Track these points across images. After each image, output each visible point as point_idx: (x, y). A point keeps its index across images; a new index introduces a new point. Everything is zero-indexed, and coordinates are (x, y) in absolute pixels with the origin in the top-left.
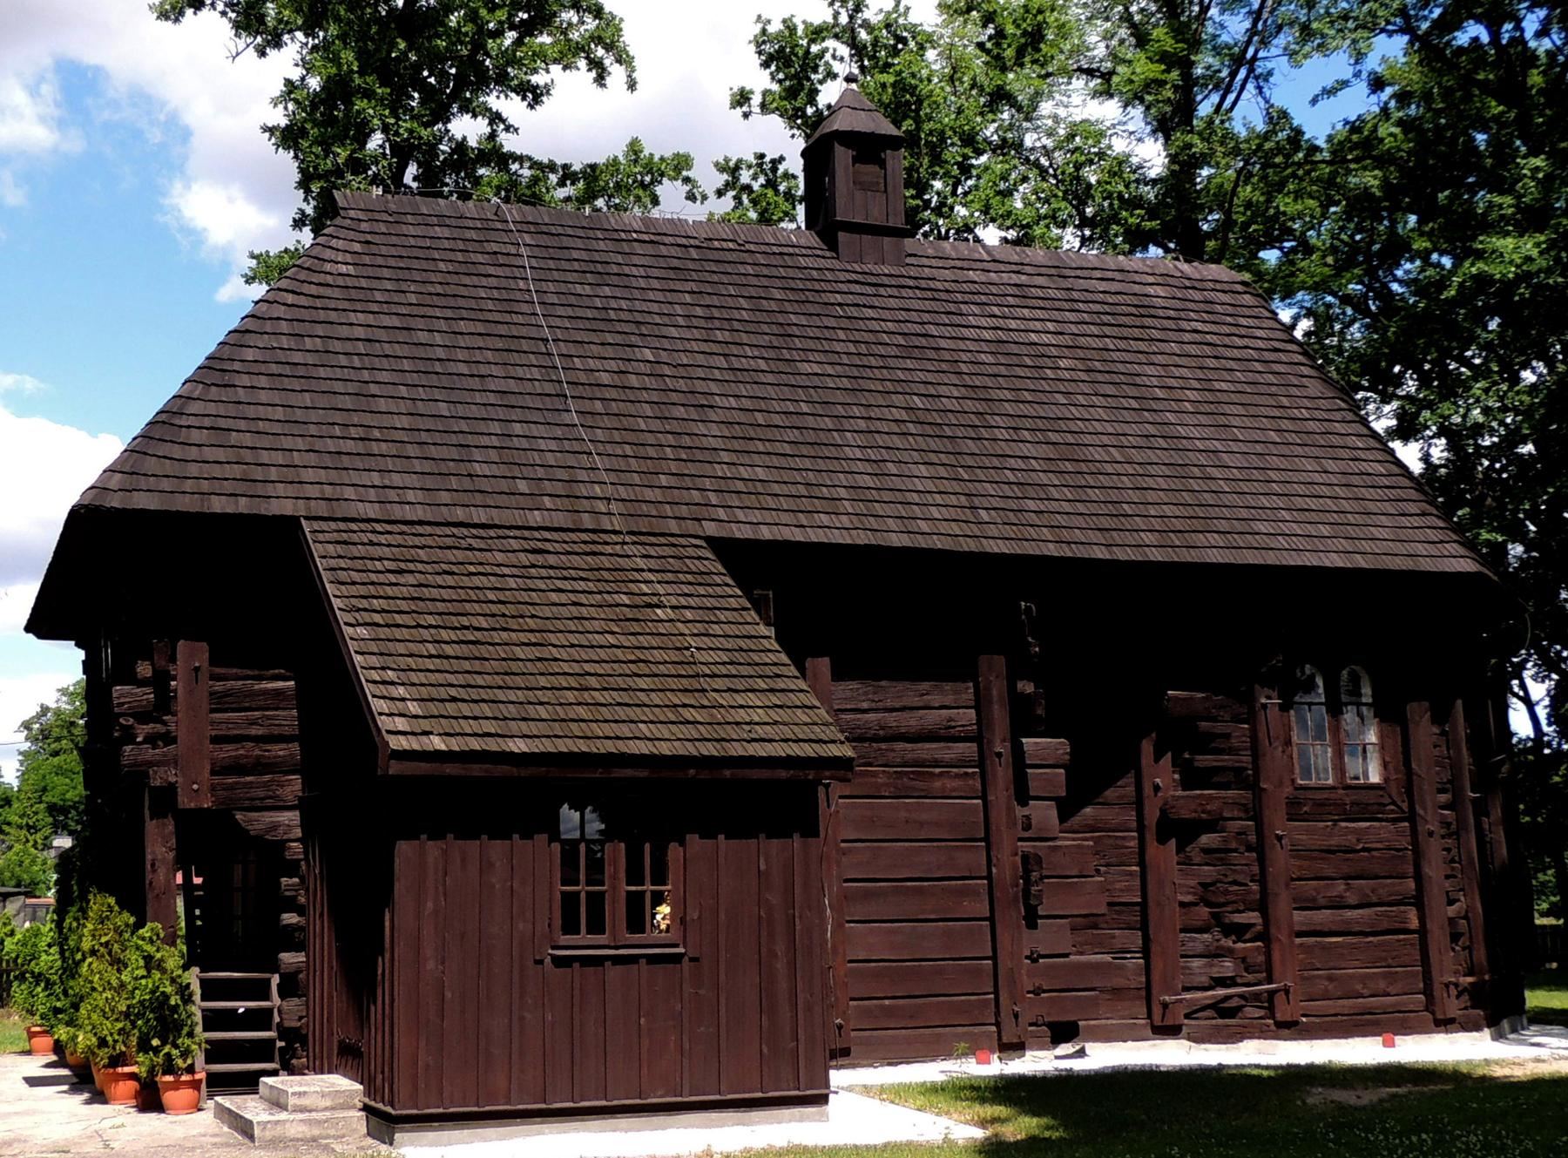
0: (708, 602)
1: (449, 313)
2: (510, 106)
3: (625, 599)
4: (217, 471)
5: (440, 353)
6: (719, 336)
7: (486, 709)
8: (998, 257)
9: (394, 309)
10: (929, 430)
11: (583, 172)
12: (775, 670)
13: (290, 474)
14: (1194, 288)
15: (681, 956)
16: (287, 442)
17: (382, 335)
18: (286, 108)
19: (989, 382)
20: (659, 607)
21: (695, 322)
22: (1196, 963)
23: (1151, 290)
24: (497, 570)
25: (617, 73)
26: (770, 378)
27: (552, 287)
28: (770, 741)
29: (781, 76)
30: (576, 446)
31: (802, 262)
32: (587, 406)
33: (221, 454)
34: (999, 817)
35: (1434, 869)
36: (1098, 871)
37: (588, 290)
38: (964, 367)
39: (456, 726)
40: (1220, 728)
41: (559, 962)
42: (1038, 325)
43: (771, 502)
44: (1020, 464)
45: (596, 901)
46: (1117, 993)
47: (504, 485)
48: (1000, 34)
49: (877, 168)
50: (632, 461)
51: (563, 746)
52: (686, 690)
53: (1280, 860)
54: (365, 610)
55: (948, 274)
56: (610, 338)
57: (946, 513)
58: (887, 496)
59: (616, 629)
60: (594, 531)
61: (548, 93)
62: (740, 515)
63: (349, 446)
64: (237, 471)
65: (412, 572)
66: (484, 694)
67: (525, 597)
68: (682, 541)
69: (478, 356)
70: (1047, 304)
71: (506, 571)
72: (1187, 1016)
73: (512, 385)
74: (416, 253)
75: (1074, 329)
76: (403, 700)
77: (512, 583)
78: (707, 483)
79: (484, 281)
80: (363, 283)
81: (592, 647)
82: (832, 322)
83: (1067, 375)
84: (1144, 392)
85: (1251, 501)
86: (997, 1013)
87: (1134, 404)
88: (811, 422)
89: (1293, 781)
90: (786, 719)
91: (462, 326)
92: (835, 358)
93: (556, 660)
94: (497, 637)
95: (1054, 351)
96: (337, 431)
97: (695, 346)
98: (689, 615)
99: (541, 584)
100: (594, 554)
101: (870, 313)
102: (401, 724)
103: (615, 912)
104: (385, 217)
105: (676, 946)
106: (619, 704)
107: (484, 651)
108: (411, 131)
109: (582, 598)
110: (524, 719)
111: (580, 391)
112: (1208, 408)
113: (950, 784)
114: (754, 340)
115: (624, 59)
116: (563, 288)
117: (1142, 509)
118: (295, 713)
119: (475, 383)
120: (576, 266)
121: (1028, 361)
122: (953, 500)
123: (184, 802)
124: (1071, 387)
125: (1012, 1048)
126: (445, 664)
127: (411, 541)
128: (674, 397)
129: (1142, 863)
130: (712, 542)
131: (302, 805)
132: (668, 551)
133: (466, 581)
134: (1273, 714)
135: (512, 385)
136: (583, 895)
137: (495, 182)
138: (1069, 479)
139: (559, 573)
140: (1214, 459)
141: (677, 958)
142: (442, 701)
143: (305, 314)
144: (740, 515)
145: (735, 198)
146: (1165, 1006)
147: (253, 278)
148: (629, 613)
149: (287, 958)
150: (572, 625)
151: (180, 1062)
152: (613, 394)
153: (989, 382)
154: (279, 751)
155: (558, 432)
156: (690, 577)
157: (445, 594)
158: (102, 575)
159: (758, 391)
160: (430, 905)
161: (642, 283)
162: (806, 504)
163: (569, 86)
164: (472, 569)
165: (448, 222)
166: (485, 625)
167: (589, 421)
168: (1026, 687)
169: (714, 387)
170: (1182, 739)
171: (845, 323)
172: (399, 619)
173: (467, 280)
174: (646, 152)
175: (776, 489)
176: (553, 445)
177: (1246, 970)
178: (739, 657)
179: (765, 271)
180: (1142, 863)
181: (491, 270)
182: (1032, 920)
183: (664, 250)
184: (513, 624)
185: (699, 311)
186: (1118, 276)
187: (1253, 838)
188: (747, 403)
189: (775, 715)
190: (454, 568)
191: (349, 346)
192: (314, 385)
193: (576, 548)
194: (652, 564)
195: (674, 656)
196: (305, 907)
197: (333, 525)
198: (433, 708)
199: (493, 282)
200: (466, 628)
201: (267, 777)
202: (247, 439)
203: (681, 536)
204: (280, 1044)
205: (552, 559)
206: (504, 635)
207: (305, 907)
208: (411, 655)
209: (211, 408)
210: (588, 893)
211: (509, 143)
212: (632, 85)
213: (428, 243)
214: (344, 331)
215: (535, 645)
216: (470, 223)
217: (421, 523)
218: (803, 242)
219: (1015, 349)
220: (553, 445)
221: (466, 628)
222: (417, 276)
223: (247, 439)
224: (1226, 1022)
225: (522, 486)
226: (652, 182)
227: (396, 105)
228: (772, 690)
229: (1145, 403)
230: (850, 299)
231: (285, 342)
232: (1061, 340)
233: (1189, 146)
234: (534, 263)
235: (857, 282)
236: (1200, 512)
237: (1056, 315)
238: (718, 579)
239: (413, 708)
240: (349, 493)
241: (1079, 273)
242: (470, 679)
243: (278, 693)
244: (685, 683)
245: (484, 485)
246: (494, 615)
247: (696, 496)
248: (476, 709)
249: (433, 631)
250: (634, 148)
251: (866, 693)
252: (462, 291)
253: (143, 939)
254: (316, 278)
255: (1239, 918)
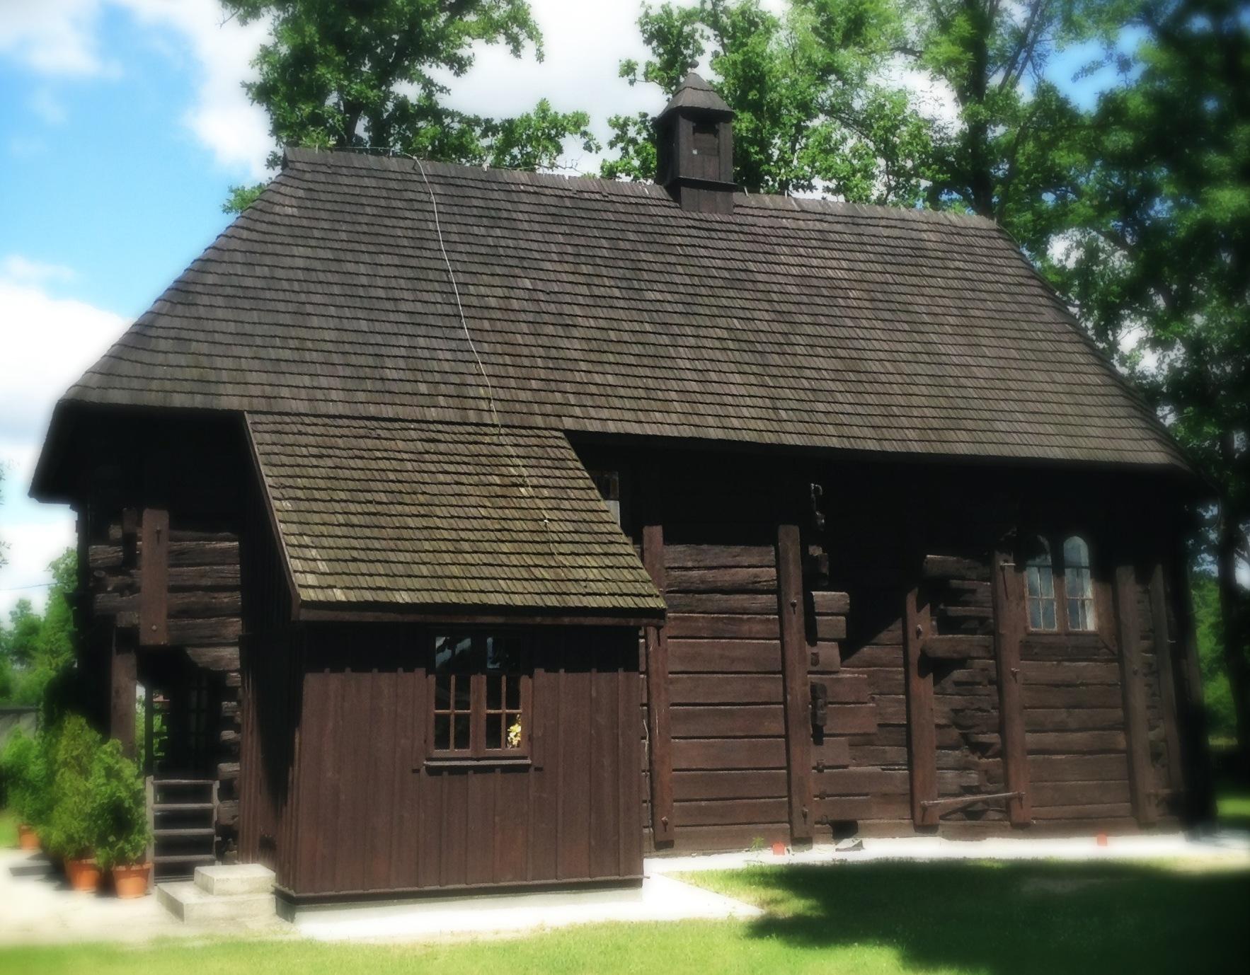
0: (562, 483)
1: (372, 248)
2: (439, 73)
3: (497, 480)
4: (178, 373)
5: (364, 280)
6: (584, 269)
7: (380, 568)
8: (806, 208)
9: (329, 244)
10: (744, 346)
11: (503, 126)
12: (610, 538)
13: (238, 376)
14: (959, 234)
15: (528, 766)
16: (237, 351)
17: (317, 265)
18: (261, 69)
19: (793, 308)
20: (522, 486)
21: (566, 258)
22: (950, 774)
23: (924, 236)
24: (399, 456)
25: (529, 47)
26: (622, 303)
27: (454, 228)
28: (600, 595)
29: (661, 51)
30: (467, 356)
31: (653, 210)
32: (476, 324)
33: (183, 360)
34: (793, 654)
35: (1139, 698)
36: (873, 699)
37: (483, 231)
38: (775, 297)
39: (354, 581)
40: (967, 585)
41: (433, 771)
42: (834, 263)
43: (617, 402)
44: (814, 374)
45: (463, 721)
46: (887, 798)
47: (408, 387)
48: (830, 22)
49: (712, 137)
50: (510, 369)
51: (438, 598)
52: (539, 554)
53: (1016, 693)
54: (291, 487)
55: (766, 222)
56: (498, 270)
57: (754, 413)
58: (709, 399)
59: (488, 504)
60: (477, 425)
61: (470, 64)
62: (593, 412)
63: (287, 354)
64: (195, 373)
65: (330, 456)
66: (379, 556)
67: (418, 477)
68: (547, 433)
69: (393, 283)
70: (843, 246)
71: (405, 456)
72: (942, 817)
73: (419, 307)
74: (349, 199)
75: (862, 266)
76: (315, 560)
77: (409, 466)
78: (568, 387)
79: (402, 223)
80: (305, 223)
81: (468, 518)
82: (673, 259)
83: (855, 303)
84: (915, 317)
85: (993, 405)
86: (790, 814)
87: (906, 327)
88: (652, 338)
89: (1026, 628)
90: (615, 577)
91: (383, 259)
92: (673, 288)
93: (438, 528)
94: (395, 509)
95: (846, 284)
96: (278, 342)
97: (565, 277)
98: (546, 492)
99: (432, 468)
100: (476, 443)
101: (703, 252)
102: (311, 579)
103: (478, 730)
104: (324, 169)
105: (525, 758)
106: (485, 564)
107: (383, 521)
108: (360, 92)
109: (464, 479)
110: (409, 576)
111: (473, 312)
112: (964, 331)
113: (757, 628)
114: (612, 272)
115: (534, 35)
116: (464, 229)
117: (907, 411)
118: (238, 567)
119: (389, 305)
120: (475, 211)
121: (825, 292)
122: (760, 402)
123: (147, 639)
124: (856, 313)
125: (802, 840)
126: (351, 532)
127: (333, 431)
128: (546, 318)
129: (907, 692)
130: (569, 434)
131: (243, 643)
132: (534, 441)
133: (373, 464)
134: (1010, 575)
135: (419, 307)
136: (452, 717)
137: (430, 134)
138: (852, 387)
139: (446, 458)
140: (965, 372)
141: (525, 768)
142: (346, 561)
143: (257, 247)
144: (593, 412)
145: (622, 149)
146: (925, 809)
147: (230, 209)
148: (498, 490)
149: (227, 768)
150: (453, 501)
151: (131, 854)
152: (498, 315)
153: (793, 308)
154: (225, 598)
155: (453, 345)
156: (549, 463)
157: (356, 474)
158: (92, 451)
159: (612, 313)
160: (331, 725)
161: (526, 226)
162: (644, 404)
163: (488, 57)
164: (378, 454)
165: (375, 174)
166: (385, 500)
167: (478, 336)
168: (816, 551)
169: (577, 311)
170: (939, 593)
171: (683, 260)
172: (317, 494)
173: (388, 222)
174: (552, 111)
175: (622, 392)
176: (449, 355)
177: (988, 781)
178: (583, 527)
179: (623, 218)
180: (907, 692)
181: (408, 214)
182: (818, 736)
183: (545, 200)
184: (407, 499)
185: (570, 249)
186: (899, 224)
187: (993, 673)
188: (602, 323)
189: (607, 574)
190: (365, 454)
191: (291, 274)
192: (261, 304)
193: (462, 438)
194: (521, 451)
195: (531, 526)
196: (241, 728)
197: (270, 418)
198: (339, 567)
199: (408, 223)
200: (370, 502)
201: (213, 620)
202: (205, 348)
203: (546, 429)
204: (217, 839)
205: (442, 447)
206: (399, 508)
207: (241, 728)
208: (324, 524)
209: (177, 323)
210: (457, 716)
211: (443, 101)
212: (540, 57)
213: (358, 191)
214: (288, 262)
215: (423, 516)
216: (393, 176)
217: (341, 417)
218: (654, 195)
219: (815, 282)
220: (449, 355)
221: (370, 502)
222: (348, 218)
223: (205, 348)
224: (973, 820)
225: (423, 388)
226: (556, 135)
227: (350, 70)
228: (606, 554)
229: (916, 327)
230: (688, 241)
231: (239, 270)
232: (853, 275)
233: (978, 113)
234: (442, 208)
235: (694, 227)
236: (952, 413)
237: (849, 255)
238: (571, 464)
239: (322, 566)
240: (285, 392)
241: (869, 221)
242: (370, 543)
243: (224, 551)
244: (539, 548)
245: (395, 387)
246: (392, 492)
247: (558, 397)
248: (373, 568)
249: (343, 504)
250: (543, 109)
251: (691, 555)
252: (383, 231)
253: (105, 753)
254: (267, 218)
255: (984, 738)
